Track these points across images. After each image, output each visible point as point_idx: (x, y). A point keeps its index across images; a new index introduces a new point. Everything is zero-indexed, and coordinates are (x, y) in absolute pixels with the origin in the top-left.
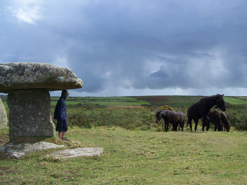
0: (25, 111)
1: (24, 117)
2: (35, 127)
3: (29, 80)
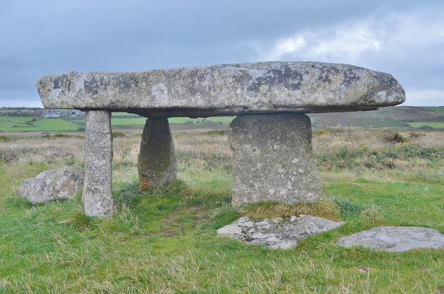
0: (265, 156)
1: (264, 168)
2: (284, 185)
3: (315, 99)
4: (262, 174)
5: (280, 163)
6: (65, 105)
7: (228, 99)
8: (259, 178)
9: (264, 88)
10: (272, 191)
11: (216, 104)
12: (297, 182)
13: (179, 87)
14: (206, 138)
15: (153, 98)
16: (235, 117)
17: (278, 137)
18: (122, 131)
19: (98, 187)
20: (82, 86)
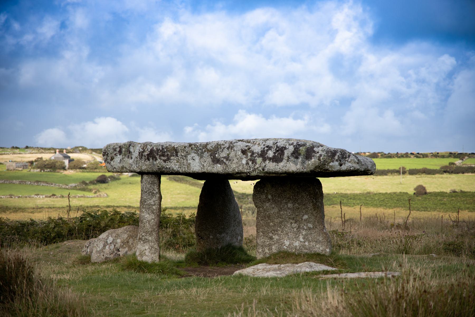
2: (297, 238)
4: (279, 229)
5: (293, 219)
8: (277, 231)
10: (287, 243)
11: (230, 170)
13: (207, 158)
14: (14, 158)
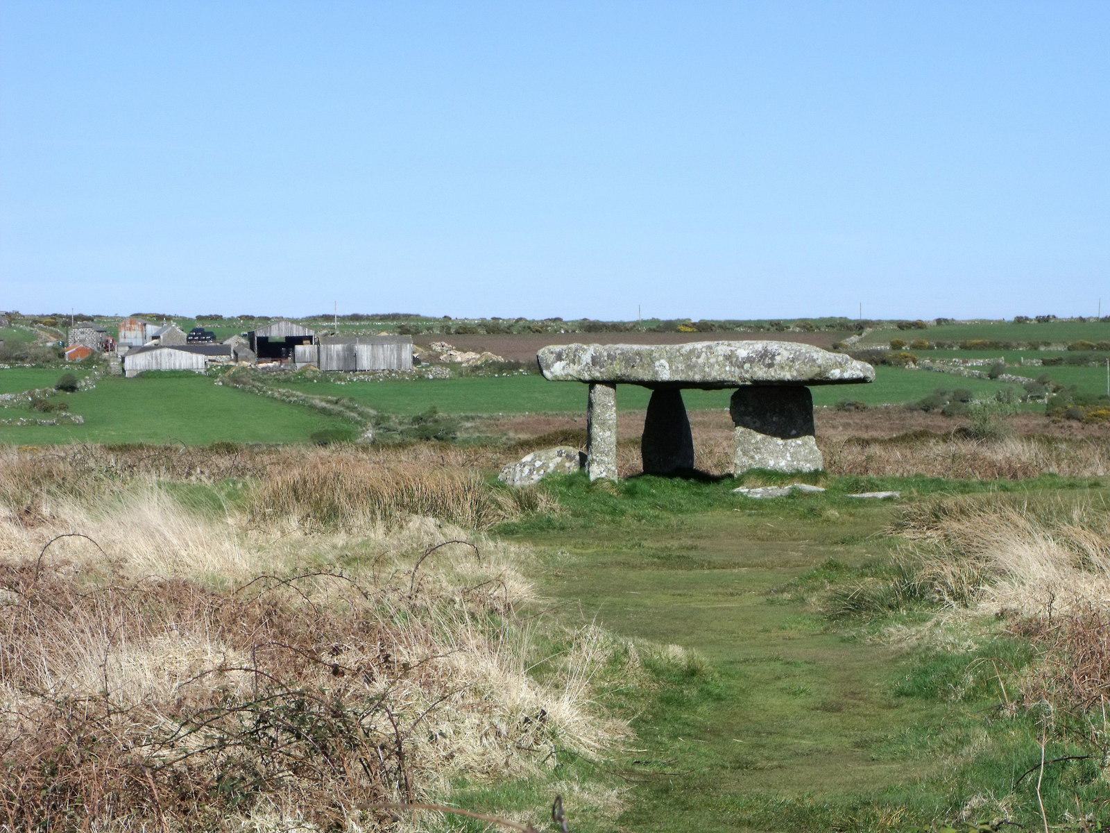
2: (784, 457)
3: (784, 376)
6: (570, 378)
7: (719, 375)
9: (747, 366)
12: (795, 453)
15: (540, 555)
16: (737, 389)
17: (777, 410)
18: (919, 421)
19: (603, 458)
20: (589, 361)
